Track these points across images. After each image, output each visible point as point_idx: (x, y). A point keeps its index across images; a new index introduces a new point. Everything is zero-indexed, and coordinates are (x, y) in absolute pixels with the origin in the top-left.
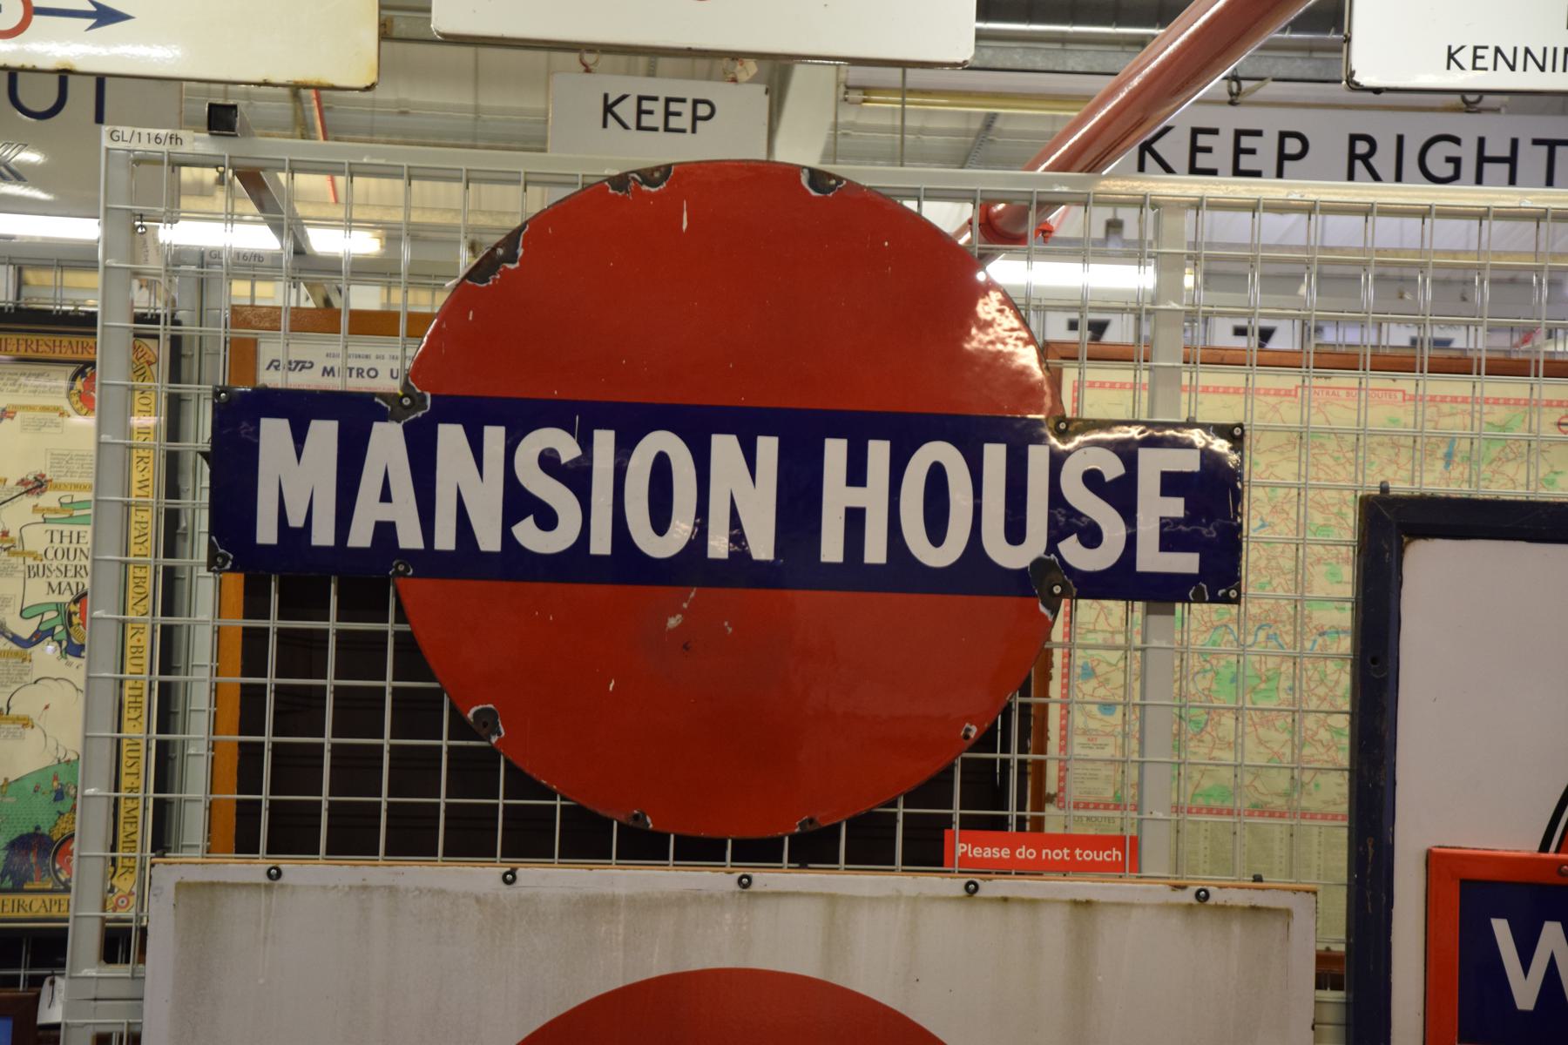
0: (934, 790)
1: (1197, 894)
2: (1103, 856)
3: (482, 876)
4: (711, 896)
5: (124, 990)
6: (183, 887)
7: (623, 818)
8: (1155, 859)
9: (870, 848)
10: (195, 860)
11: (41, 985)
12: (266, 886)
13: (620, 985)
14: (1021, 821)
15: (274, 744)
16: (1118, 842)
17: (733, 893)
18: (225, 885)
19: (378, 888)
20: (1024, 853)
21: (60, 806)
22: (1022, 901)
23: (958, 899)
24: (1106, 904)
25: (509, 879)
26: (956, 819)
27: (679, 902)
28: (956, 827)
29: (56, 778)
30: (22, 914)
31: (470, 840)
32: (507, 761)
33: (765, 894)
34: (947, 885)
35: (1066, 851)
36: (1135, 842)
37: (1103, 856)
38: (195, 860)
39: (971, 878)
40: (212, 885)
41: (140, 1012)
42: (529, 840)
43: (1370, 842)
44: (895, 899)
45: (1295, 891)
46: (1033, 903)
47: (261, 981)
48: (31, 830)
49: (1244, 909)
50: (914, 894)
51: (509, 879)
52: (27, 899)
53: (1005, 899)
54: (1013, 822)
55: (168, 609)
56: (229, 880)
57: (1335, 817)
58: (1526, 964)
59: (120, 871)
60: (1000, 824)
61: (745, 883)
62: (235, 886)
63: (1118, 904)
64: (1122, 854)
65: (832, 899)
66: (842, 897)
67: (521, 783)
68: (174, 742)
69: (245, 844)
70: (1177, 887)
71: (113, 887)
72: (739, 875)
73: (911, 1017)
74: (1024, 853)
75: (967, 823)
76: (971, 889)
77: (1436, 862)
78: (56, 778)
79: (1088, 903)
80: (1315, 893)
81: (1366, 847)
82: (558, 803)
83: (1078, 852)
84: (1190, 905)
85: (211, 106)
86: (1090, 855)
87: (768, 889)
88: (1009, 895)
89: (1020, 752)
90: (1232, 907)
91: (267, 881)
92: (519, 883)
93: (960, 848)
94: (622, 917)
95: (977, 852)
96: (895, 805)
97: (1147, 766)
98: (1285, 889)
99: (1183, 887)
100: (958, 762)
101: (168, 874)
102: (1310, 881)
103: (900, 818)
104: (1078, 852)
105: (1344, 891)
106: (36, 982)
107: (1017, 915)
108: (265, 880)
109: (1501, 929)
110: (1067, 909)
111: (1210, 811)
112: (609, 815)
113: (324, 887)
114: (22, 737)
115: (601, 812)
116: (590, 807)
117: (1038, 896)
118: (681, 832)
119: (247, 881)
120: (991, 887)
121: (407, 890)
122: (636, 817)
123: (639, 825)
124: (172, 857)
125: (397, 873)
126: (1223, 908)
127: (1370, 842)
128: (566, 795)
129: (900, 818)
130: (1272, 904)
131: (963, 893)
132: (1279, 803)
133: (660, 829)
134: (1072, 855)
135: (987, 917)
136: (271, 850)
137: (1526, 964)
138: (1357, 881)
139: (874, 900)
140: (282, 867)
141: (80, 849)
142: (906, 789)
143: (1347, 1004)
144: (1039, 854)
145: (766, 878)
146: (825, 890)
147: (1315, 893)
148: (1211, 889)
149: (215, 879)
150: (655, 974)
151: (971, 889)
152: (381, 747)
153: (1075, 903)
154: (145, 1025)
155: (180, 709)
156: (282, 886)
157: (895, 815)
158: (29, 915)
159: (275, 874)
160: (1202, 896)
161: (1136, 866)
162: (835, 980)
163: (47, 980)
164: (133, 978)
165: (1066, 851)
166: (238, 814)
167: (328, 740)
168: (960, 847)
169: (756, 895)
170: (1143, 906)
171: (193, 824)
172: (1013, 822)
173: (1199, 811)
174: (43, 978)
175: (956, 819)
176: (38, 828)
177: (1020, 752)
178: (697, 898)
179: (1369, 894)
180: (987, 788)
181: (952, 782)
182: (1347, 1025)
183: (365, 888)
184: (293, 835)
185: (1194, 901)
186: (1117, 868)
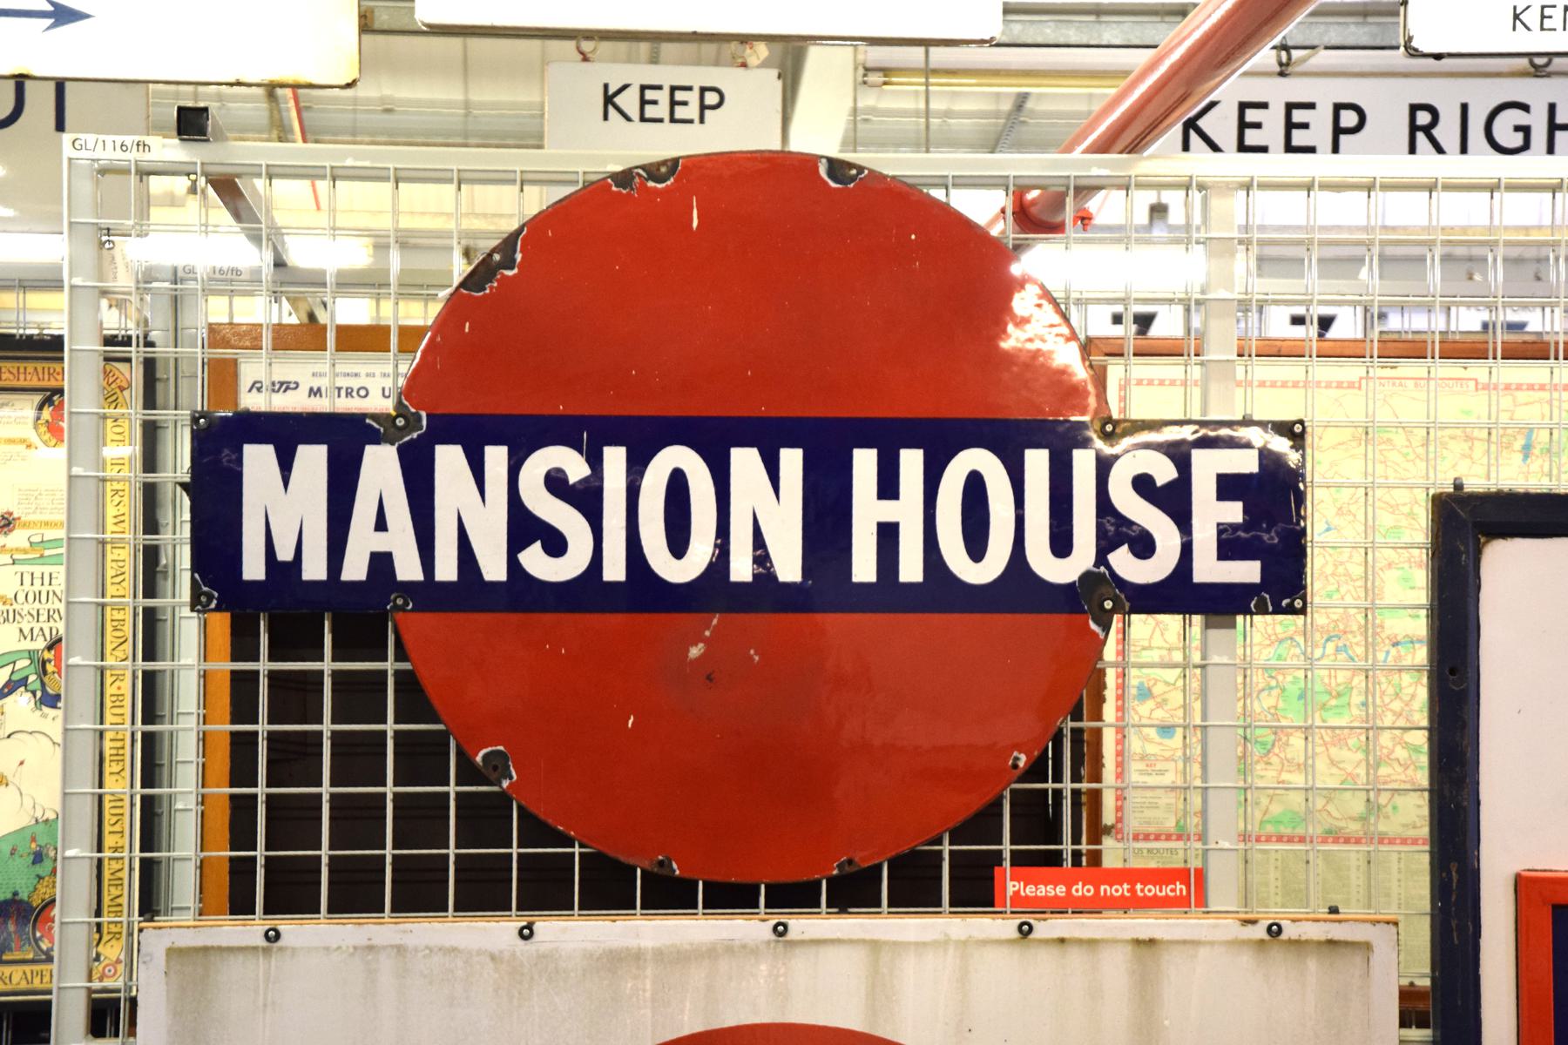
0: (982, 824)
1: (1269, 929)
2: (1167, 891)
3: (494, 932)
4: (744, 947)
6: (173, 953)
7: (647, 864)
8: (1222, 892)
9: (915, 890)
12: (265, 950)
14: (1077, 855)
16: (1181, 875)
17: (769, 942)
18: (220, 949)
19: (384, 948)
20: (1081, 890)
22: (1080, 942)
25: (526, 934)
26: (1007, 855)
27: (711, 953)
28: (1007, 864)
29: (33, 839)
31: (482, 893)
32: (520, 808)
33: (802, 943)
35: (1126, 886)
36: (1201, 875)
37: (1167, 891)
38: (184, 925)
39: (1024, 918)
40: (206, 950)
43: (1454, 867)
44: (943, 944)
45: (1375, 922)
46: (1091, 943)
48: (9, 896)
49: (1319, 943)
51: (526, 934)
53: (1062, 941)
56: (224, 944)
60: (1054, 859)
61: (780, 931)
62: (230, 950)
63: (1185, 942)
64: (1186, 887)
65: (875, 945)
66: (886, 943)
67: (535, 831)
69: (240, 905)
71: (98, 955)
72: (774, 922)
74: (1081, 890)
75: (1019, 859)
76: (1025, 931)
77: (1525, 886)
78: (33, 839)
80: (1396, 924)
81: (1449, 872)
82: (577, 850)
83: (1139, 886)
84: (1262, 941)
86: (1152, 890)
87: (806, 937)
88: (1066, 935)
90: (1307, 942)
92: (536, 938)
93: (1012, 887)
94: (649, 972)
95: (1030, 890)
96: (940, 843)
98: (1364, 921)
99: (1254, 922)
100: (1007, 793)
101: (158, 939)
102: (1391, 912)
104: (1139, 886)
107: (1075, 956)
108: (262, 943)
110: (1129, 948)
111: (1280, 839)
112: (631, 861)
113: (327, 949)
115: (622, 858)
116: (611, 853)
119: (243, 944)
120: (1048, 928)
121: (416, 950)
122: (661, 863)
123: (664, 872)
126: (1298, 944)
127: (1454, 867)
128: (585, 841)
130: (1350, 938)
131: (1016, 935)
132: (1354, 828)
133: (687, 875)
134: (1132, 890)
135: (1045, 959)
136: (269, 910)
139: (920, 946)
140: (281, 928)
142: (951, 825)
145: (802, 925)
146: (868, 937)
147: (1396, 924)
148: (1283, 923)
149: (209, 943)
151: (1025, 931)
153: (1138, 942)
156: (281, 949)
159: (273, 936)
160: (1275, 931)
161: (1202, 901)
165: (1126, 886)
168: (1012, 885)
170: (1211, 943)
171: (184, 884)
173: (1268, 840)
175: (1007, 855)
176: (16, 894)
178: (731, 949)
179: (1454, 923)
180: (1038, 820)
181: (1001, 815)
183: (371, 948)
184: (291, 893)
185: (1266, 937)
186: (1181, 902)
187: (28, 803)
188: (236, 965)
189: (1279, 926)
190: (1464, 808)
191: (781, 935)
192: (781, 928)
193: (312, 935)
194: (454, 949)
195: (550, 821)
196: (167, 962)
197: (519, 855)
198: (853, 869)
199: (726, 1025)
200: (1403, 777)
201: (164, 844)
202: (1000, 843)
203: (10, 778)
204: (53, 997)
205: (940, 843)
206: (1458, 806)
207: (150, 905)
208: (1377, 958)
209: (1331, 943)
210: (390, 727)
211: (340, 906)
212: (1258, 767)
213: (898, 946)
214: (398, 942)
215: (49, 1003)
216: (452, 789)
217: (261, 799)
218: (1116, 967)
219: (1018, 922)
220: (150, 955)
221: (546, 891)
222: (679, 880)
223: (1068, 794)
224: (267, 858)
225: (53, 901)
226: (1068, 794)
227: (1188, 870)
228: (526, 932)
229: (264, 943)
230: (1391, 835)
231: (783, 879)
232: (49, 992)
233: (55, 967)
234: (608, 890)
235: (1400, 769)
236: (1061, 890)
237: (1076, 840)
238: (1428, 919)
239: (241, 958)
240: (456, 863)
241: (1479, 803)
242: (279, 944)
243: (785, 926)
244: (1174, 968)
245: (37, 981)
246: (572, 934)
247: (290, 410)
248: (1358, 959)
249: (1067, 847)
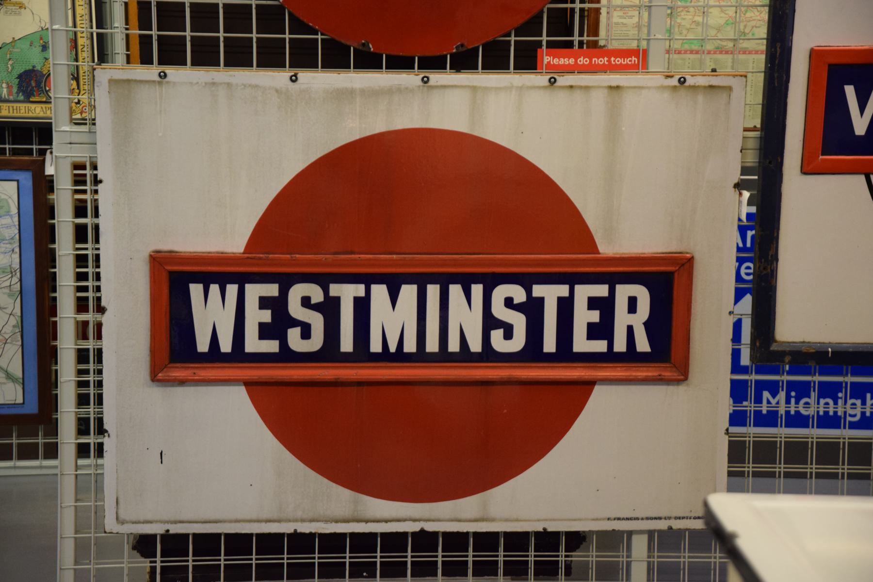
0: (532, 26)
1: (679, 80)
2: (627, 61)
3: (279, 78)
4: (407, 88)
5: (85, 138)
6: (112, 82)
7: (356, 45)
8: (657, 61)
9: (496, 61)
11: (45, 154)
12: (159, 82)
13: (358, 137)
14: (581, 43)
16: (635, 52)
17: (419, 87)
18: (136, 81)
19: (221, 84)
20: (582, 61)
22: (581, 87)
23: (545, 87)
25: (294, 79)
26: (544, 43)
27: (390, 92)
28: (544, 47)
29: (41, 39)
30: (31, 115)
31: (271, 58)
32: (290, 14)
34: (539, 79)
35: (606, 59)
36: (645, 52)
37: (627, 61)
38: (118, 69)
39: (552, 75)
41: (95, 151)
43: (778, 45)
44: (509, 88)
45: (734, 76)
46: (587, 88)
47: (160, 134)
48: (31, 68)
49: (705, 87)
50: (520, 85)
51: (294, 79)
52: (33, 106)
53: (571, 87)
54: (576, 44)
56: (138, 78)
58: (862, 109)
59: (82, 92)
60: (569, 45)
61: (425, 80)
62: (141, 82)
63: (635, 87)
64: (637, 59)
65: (474, 89)
66: (480, 87)
67: (298, 26)
69: (146, 60)
70: (668, 77)
71: (79, 101)
72: (422, 76)
73: (518, 152)
75: (551, 45)
76: (552, 82)
77: (816, 55)
78: (41, 39)
79: (618, 87)
80: (746, 76)
81: (776, 48)
82: (319, 37)
83: (613, 59)
84: (675, 87)
85: (260, 308)
86: (619, 61)
87: (439, 84)
88: (573, 84)
91: (159, 79)
92: (299, 81)
93: (546, 59)
94: (358, 100)
95: (556, 61)
97: (653, 8)
98: (729, 75)
99: (672, 77)
100: (545, 10)
101: (104, 74)
102: (742, 70)
103: (513, 43)
104: (613, 59)
106: (42, 153)
107: (578, 95)
108: (158, 79)
109: (850, 91)
110: (606, 91)
111: (691, 52)
112: (348, 43)
113: (191, 83)
114: (20, 14)
115: (343, 41)
116: (337, 39)
117: (590, 84)
118: (388, 53)
119: (148, 79)
120: (564, 80)
121: (237, 85)
122: (364, 45)
123: (365, 49)
124: (104, 65)
125: (231, 76)
126: (694, 88)
127: (778, 45)
128: (324, 32)
129: (513, 43)
130: (721, 84)
133: (378, 51)
134: (609, 61)
135: (561, 98)
136: (160, 63)
138: (770, 68)
139: (498, 89)
140: (167, 71)
141: (53, 59)
142: (516, 26)
143: (761, 138)
145: (437, 78)
146: (471, 84)
147: (746, 76)
148: (687, 77)
149: (130, 77)
150: (377, 131)
151: (552, 82)
153: (611, 87)
154: (99, 157)
156: (168, 82)
157: (510, 41)
158: (34, 115)
159: (163, 76)
160: (682, 81)
161: (645, 66)
162: (476, 133)
163: (49, 151)
164: (90, 132)
165: (606, 59)
166: (140, 43)
168: (546, 58)
170: (649, 88)
171: (119, 46)
172: (576, 44)
173: (686, 52)
174: (46, 150)
175: (544, 43)
176: (34, 67)
178: (400, 90)
179: (776, 75)
182: (760, 149)
183: (214, 84)
184: (172, 55)
187: (37, 19)
189: (685, 79)
191: (426, 82)
192: (425, 79)
194: (257, 86)
195: (305, 20)
196: (109, 86)
198: (464, 49)
199: (397, 128)
200: (759, 18)
201: (109, 26)
202: (541, 36)
203: (26, 5)
207: (103, 56)
208: (734, 94)
209: (711, 87)
210: (221, 35)
211: (197, 62)
212: (682, 14)
213: (486, 89)
214: (227, 81)
215: (51, 123)
216: (254, 35)
217: (155, 38)
218: (599, 99)
219: (549, 77)
220: (100, 82)
221: (304, 58)
223: (577, 11)
224: (159, 36)
225: (49, 75)
226: (577, 11)
228: (294, 78)
229: (158, 79)
230: (750, 49)
231: (428, 54)
232: (51, 119)
233: (52, 105)
234: (336, 58)
235: (757, 14)
236: (572, 61)
237: (581, 34)
238: (763, 74)
240: (257, 42)
241: (794, 11)
242: (166, 80)
243: (428, 78)
244: (629, 100)
246: (319, 80)
247: (149, 334)
248: (724, 95)
249: (576, 38)
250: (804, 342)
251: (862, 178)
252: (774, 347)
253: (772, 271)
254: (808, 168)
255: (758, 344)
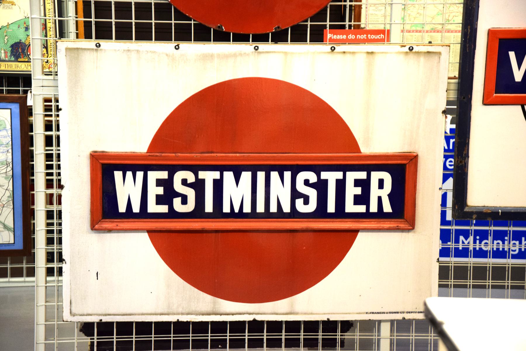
0: (320, 16)
1: (409, 48)
2: (378, 37)
6: (67, 49)
7: (214, 27)
8: (395, 36)
9: (299, 37)
10: (72, 41)
12: (96, 50)
14: (350, 26)
15: (96, 22)
16: (382, 32)
18: (82, 49)
20: (351, 37)
21: (27, 33)
22: (350, 53)
24: (378, 53)
25: (177, 48)
26: (328, 26)
28: (328, 29)
29: (25, 23)
30: (18, 69)
31: (163, 35)
32: (175, 8)
33: (263, 52)
35: (365, 35)
36: (389, 31)
37: (378, 37)
38: (72, 41)
39: (333, 45)
40: (78, 49)
42: (183, 35)
43: (469, 27)
45: (443, 46)
46: (354, 53)
48: (19, 41)
49: (425, 53)
51: (177, 48)
52: (20, 64)
53: (344, 52)
54: (347, 26)
55: (60, 15)
56: (83, 47)
57: (456, 32)
58: (519, 67)
60: (343, 27)
62: (85, 49)
64: (383, 35)
65: (286, 53)
67: (179, 15)
68: (64, 20)
69: (88, 36)
70: (402, 46)
71: (48, 61)
74: (351, 37)
75: (331, 27)
76: (333, 49)
77: (491, 33)
78: (25, 23)
79: (372, 53)
80: (449, 46)
82: (192, 22)
83: (369, 36)
84: (407, 52)
86: (373, 37)
89: (349, 22)
91: (96, 48)
93: (329, 36)
95: (335, 37)
96: (307, 22)
99: (405, 46)
100: (329, 6)
101: (62, 45)
103: (309, 26)
104: (369, 36)
105: (459, 46)
106: (26, 92)
109: (512, 55)
110: (365, 55)
112: (210, 26)
113: (115, 50)
115: (207, 25)
116: (203, 23)
118: (234, 32)
120: (339, 48)
122: (219, 27)
123: (220, 30)
126: (418, 53)
127: (469, 27)
128: (195, 19)
129: (309, 26)
131: (330, 50)
132: (439, 27)
134: (367, 37)
136: (97, 38)
137: (519, 67)
142: (311, 16)
143: (458, 83)
144: (356, 37)
145: (263, 47)
147: (449, 46)
149: (78, 47)
151: (333, 49)
152: (132, 23)
153: (368, 53)
155: (66, 32)
156: (101, 50)
157: (307, 25)
158: (21, 69)
159: (98, 46)
160: (411, 49)
161: (388, 40)
163: (29, 91)
164: (54, 80)
165: (365, 35)
167: (113, 20)
169: (260, 53)
171: (71, 28)
172: (347, 26)
174: (28, 90)
175: (328, 26)
176: (20, 40)
177: (349, 22)
179: (467, 45)
180: (338, 14)
181: (327, 11)
182: (458, 90)
183: (129, 50)
184: (103, 33)
185: (408, 51)
186: (382, 41)
188: (87, 54)
190: (474, 9)
191: (256, 50)
192: (256, 48)
193: (112, 47)
197: (175, 23)
200: (457, 11)
201: (65, 16)
202: (326, 22)
204: (32, 73)
205: (307, 22)
206: (472, 7)
207: (62, 33)
208: (442, 57)
209: (428, 52)
215: (31, 74)
222: (224, 32)
223: (348, 6)
224: (96, 22)
226: (348, 6)
227: (385, 30)
228: (177, 47)
229: (95, 48)
230: (452, 29)
232: (31, 71)
234: (203, 35)
236: (345, 37)
237: (350, 21)
239: (89, 52)
240: (155, 26)
241: (479, 7)
242: (100, 48)
245: (29, 68)
248: (437, 57)
249: (347, 23)
250: (484, 206)
251: (520, 107)
252: (466, 209)
253: (465, 164)
254: (487, 102)
255: (457, 208)
